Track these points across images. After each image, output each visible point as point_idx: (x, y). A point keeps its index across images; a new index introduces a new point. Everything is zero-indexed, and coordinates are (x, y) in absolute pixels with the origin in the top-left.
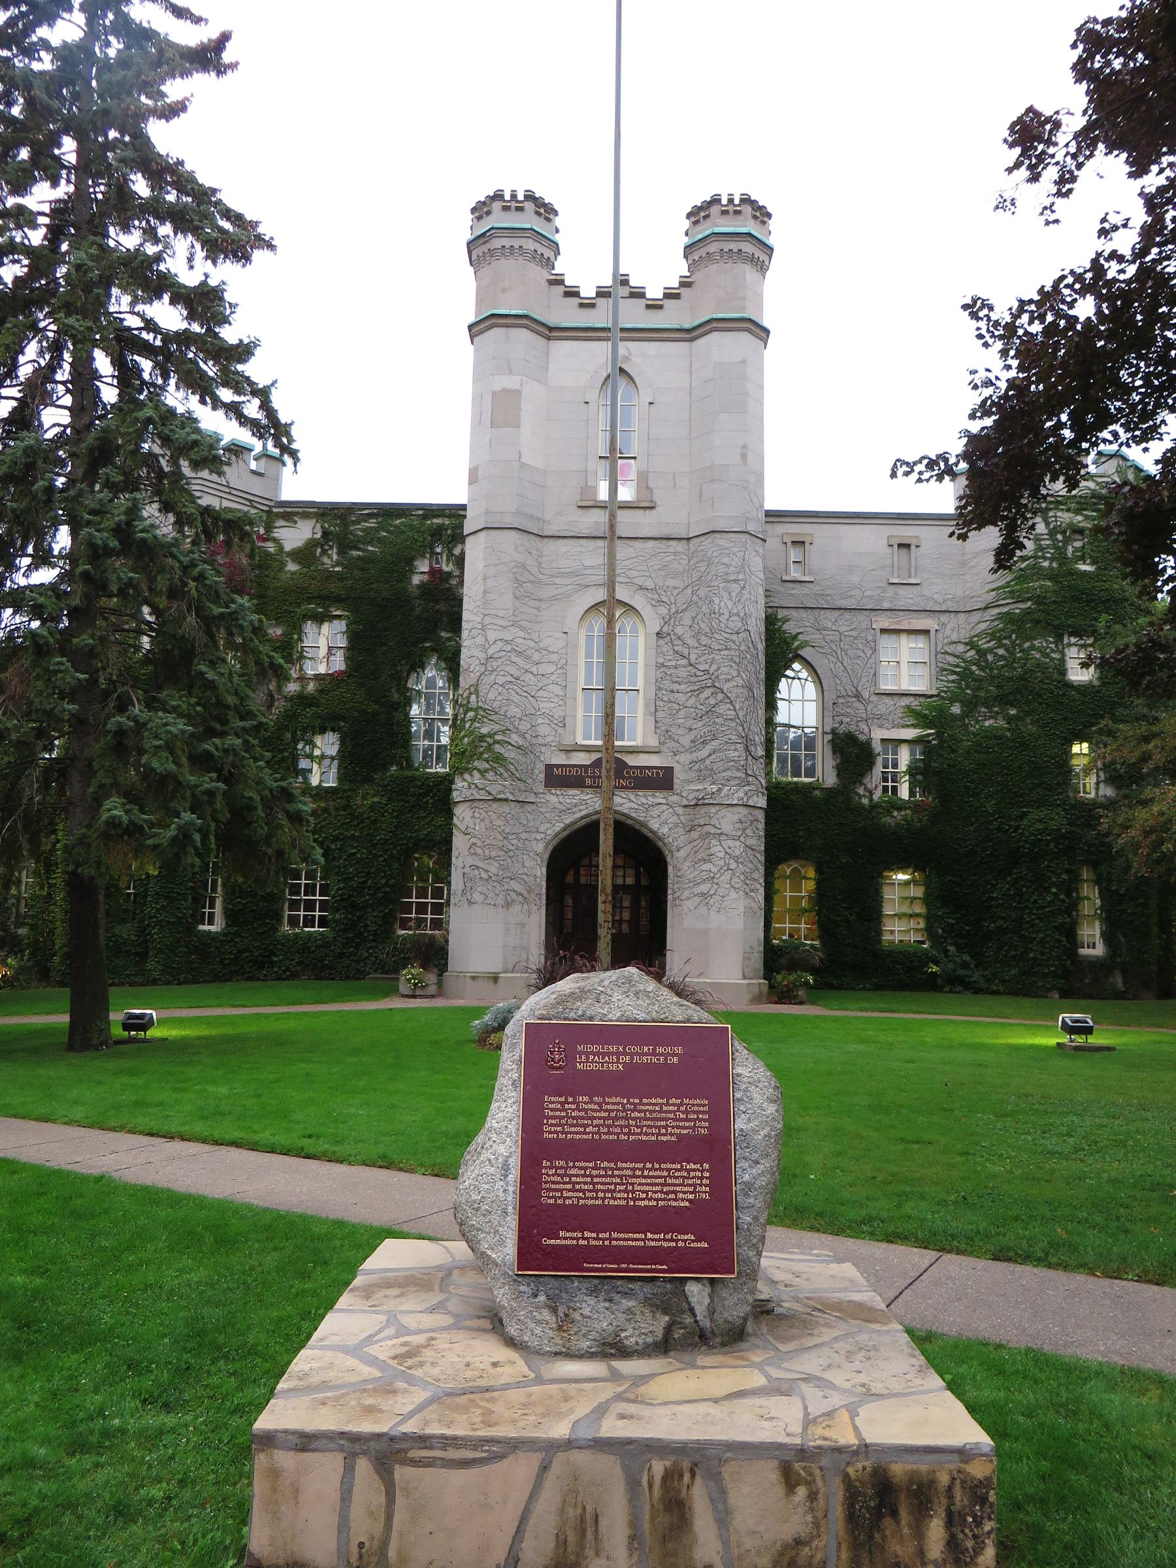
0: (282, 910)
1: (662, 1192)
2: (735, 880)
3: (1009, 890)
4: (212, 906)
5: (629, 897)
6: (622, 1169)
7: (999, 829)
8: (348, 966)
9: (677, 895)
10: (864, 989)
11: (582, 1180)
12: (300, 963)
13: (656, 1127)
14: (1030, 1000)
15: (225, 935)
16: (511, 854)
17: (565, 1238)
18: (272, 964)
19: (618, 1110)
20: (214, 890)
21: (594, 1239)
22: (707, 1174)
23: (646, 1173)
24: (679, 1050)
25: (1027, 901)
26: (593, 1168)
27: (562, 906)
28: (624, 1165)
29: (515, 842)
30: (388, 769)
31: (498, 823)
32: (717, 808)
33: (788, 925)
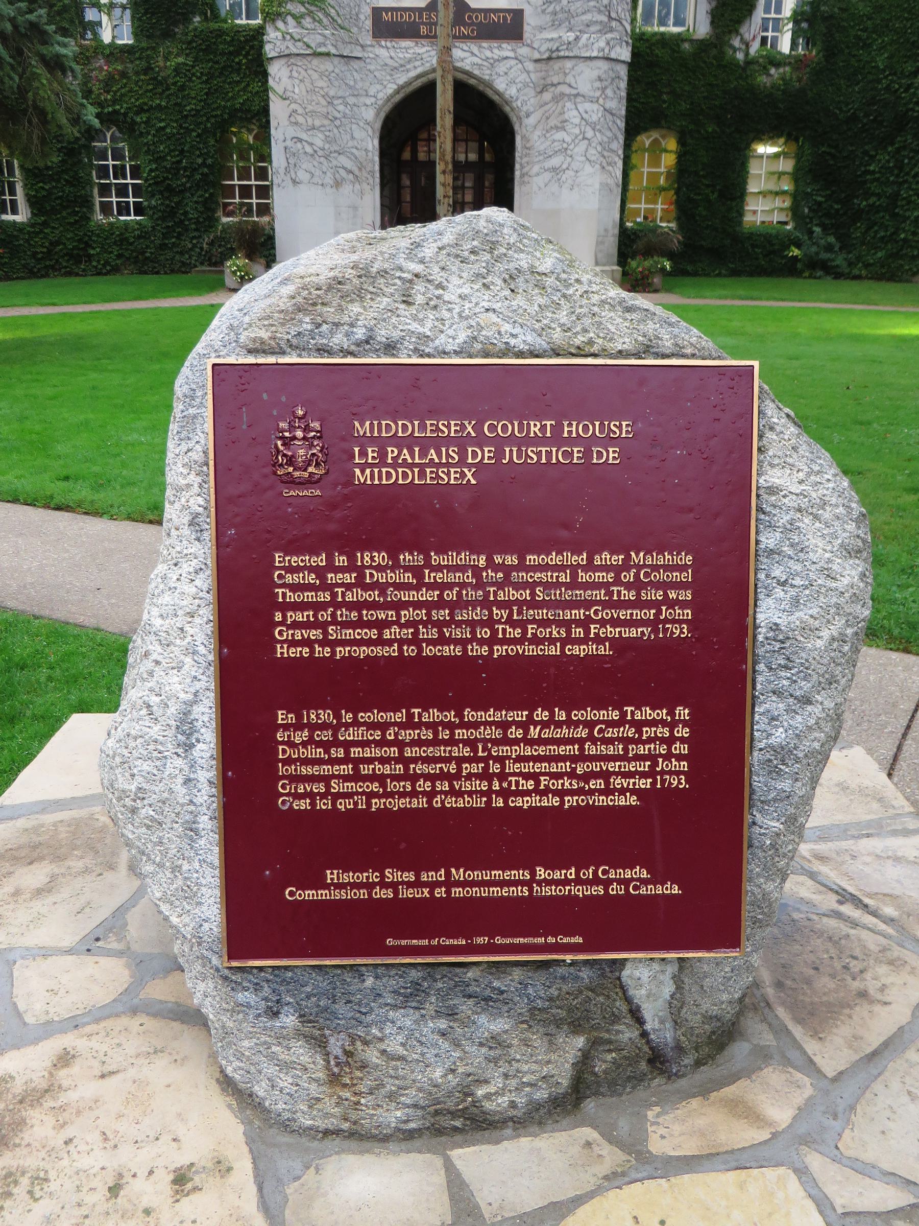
0: (92, 197)
1: (572, 775)
2: (592, 151)
3: (888, 161)
4: (12, 192)
5: (472, 175)
6: (475, 725)
7: (888, 88)
8: (172, 259)
9: (525, 170)
10: (719, 275)
11: (377, 752)
12: (119, 256)
13: (560, 623)
14: (899, 285)
15: (32, 225)
16: (337, 123)
17: (340, 886)
18: (90, 257)
19: (463, 585)
20: (11, 173)
21: (409, 885)
22: (685, 732)
23: (534, 732)
24: (623, 428)
25: (908, 174)
26: (402, 726)
27: (399, 187)
28: (481, 715)
29: (341, 108)
30: (190, 21)
31: (321, 84)
32: (573, 62)
33: (643, 206)
